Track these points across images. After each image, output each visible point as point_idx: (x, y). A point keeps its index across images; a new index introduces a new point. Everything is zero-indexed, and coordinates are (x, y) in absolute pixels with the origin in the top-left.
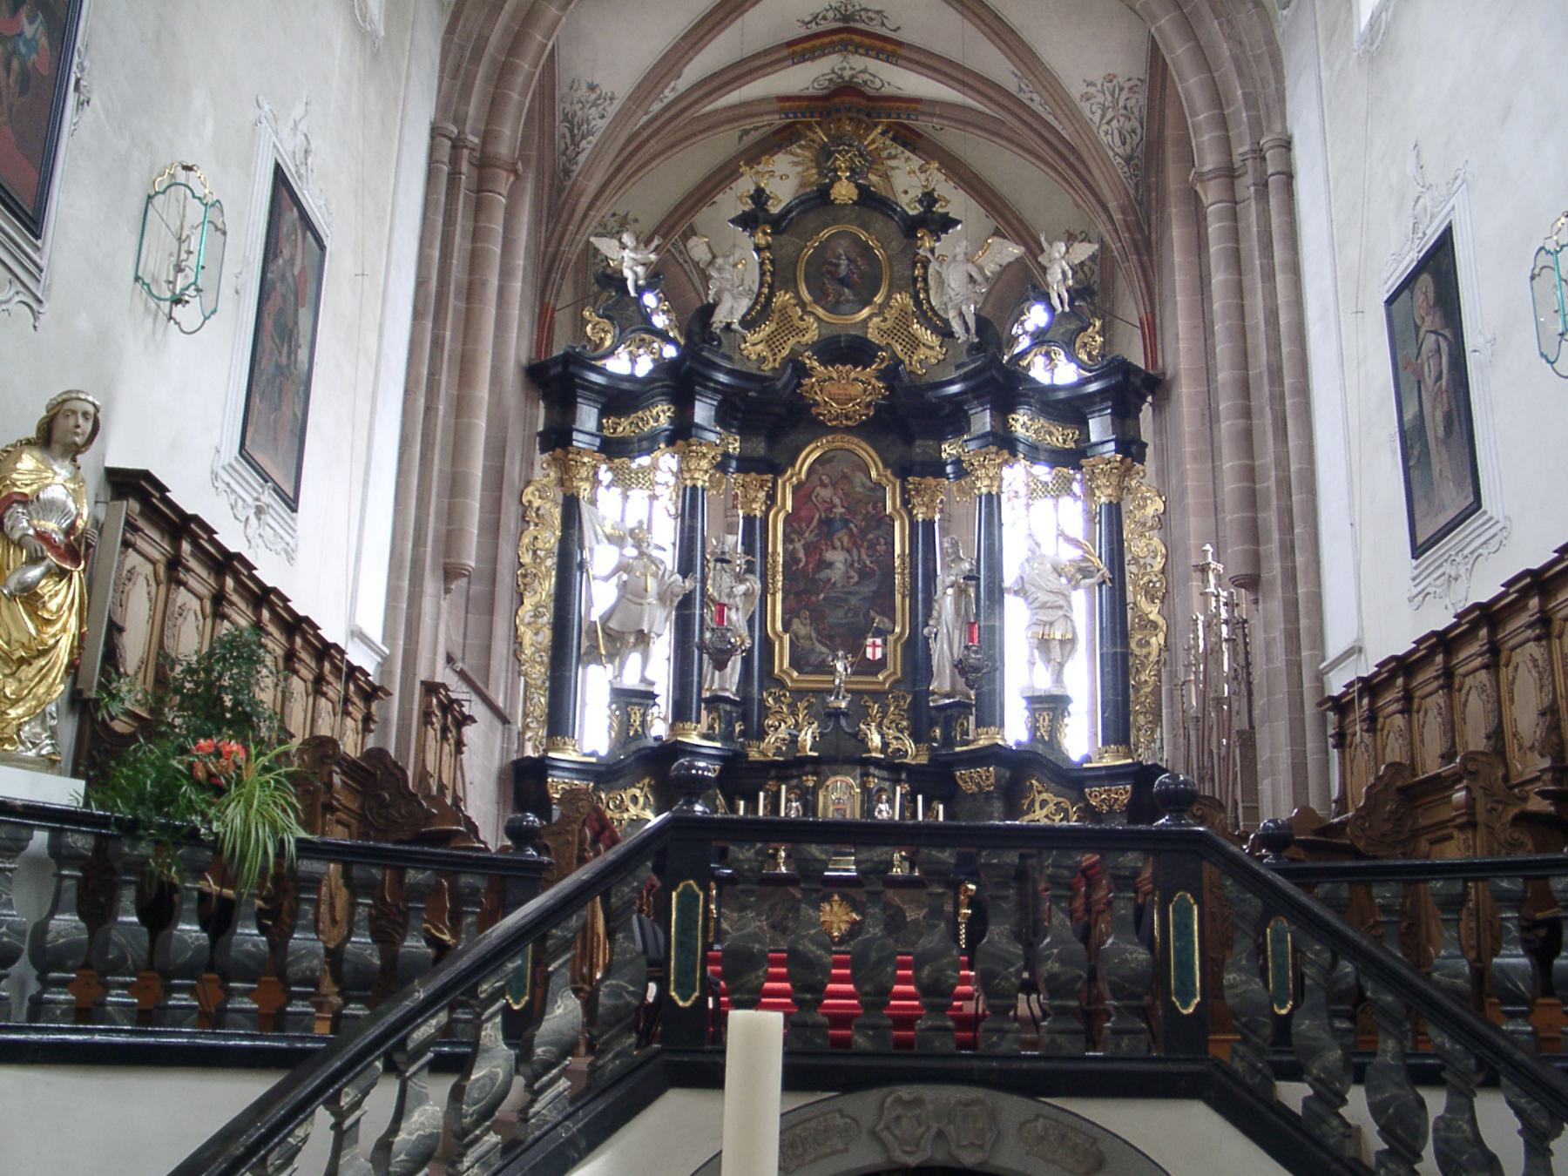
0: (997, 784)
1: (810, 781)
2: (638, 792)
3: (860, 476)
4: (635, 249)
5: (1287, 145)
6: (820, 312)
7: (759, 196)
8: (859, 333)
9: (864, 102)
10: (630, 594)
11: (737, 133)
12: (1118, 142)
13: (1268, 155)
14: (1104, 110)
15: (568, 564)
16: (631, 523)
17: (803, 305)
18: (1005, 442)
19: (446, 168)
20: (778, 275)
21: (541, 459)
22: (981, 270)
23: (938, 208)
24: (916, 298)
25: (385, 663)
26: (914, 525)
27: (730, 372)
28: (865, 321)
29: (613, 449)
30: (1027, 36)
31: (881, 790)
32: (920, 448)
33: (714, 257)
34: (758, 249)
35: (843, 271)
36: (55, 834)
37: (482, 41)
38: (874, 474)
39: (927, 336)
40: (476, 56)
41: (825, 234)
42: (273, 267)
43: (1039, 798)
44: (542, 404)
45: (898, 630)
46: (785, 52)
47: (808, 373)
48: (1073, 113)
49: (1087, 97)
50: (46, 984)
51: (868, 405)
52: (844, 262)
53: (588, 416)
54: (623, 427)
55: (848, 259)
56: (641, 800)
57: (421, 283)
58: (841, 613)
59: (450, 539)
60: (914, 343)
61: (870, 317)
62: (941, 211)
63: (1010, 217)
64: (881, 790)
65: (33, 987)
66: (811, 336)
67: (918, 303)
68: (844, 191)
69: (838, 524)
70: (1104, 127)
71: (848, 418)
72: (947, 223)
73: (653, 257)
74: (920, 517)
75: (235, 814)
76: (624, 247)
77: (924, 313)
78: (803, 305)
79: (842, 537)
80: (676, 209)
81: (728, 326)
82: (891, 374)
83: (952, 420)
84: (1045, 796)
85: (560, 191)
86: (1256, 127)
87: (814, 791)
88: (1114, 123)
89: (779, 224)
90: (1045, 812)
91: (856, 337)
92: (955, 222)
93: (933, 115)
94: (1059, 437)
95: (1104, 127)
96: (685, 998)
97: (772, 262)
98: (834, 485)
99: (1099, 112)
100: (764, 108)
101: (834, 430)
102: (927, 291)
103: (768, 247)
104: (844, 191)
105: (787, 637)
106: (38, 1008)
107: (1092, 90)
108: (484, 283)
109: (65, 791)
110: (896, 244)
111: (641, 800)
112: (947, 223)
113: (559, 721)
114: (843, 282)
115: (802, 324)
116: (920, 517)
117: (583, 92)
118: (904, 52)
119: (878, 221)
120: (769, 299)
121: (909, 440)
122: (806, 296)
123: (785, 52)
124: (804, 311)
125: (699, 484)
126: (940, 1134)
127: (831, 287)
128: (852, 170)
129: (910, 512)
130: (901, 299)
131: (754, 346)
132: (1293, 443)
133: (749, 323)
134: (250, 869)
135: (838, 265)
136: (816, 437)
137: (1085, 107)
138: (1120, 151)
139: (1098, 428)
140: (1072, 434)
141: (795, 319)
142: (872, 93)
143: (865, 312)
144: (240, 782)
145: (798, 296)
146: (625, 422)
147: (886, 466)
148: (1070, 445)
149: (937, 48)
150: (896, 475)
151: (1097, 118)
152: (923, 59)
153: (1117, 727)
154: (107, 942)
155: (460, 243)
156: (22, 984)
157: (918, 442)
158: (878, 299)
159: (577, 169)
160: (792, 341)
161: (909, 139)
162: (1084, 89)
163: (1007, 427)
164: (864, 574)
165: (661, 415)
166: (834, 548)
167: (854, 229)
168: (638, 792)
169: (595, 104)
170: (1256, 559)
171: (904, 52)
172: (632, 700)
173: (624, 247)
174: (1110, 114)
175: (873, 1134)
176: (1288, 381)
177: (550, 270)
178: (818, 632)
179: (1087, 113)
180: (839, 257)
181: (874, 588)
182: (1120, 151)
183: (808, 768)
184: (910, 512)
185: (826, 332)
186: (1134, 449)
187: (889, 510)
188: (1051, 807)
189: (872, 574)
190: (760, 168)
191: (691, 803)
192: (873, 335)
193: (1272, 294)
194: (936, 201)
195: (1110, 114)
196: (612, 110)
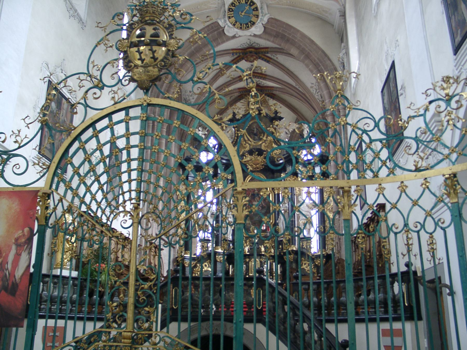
0: (294, 259)
1: (247, 260)
2: (206, 264)
4: (202, 131)
7: (234, 114)
8: (259, 147)
9: (260, 88)
11: (229, 98)
12: (320, 98)
13: (341, 111)
14: (316, 90)
19: (151, 125)
22: (288, 130)
23: (279, 115)
26: (275, 195)
27: (226, 160)
28: (261, 144)
30: (296, 73)
31: (265, 262)
34: (234, 128)
35: (255, 132)
36: (73, 281)
41: (251, 123)
42: (111, 161)
43: (304, 262)
44: (181, 170)
45: (271, 221)
46: (238, 79)
48: (309, 91)
49: (312, 87)
50: (73, 307)
51: (263, 165)
52: (255, 130)
55: (257, 129)
56: (207, 266)
58: (257, 217)
61: (262, 143)
62: (279, 115)
63: (299, 114)
64: (265, 262)
65: (70, 307)
66: (248, 149)
69: (256, 195)
70: (317, 94)
71: (258, 168)
72: (281, 118)
73: (206, 133)
74: (276, 193)
75: (103, 277)
76: (199, 131)
77: (275, 142)
84: (305, 262)
85: (184, 117)
87: (248, 262)
88: (319, 93)
90: (305, 266)
92: (283, 118)
93: (277, 91)
95: (317, 94)
96: (175, 307)
99: (315, 91)
100: (235, 91)
103: (236, 127)
106: (71, 310)
107: (313, 85)
109: (75, 274)
111: (207, 266)
112: (281, 118)
113: (187, 246)
115: (245, 146)
116: (276, 193)
117: (188, 93)
118: (267, 77)
123: (238, 79)
124: (246, 143)
125: (220, 188)
126: (216, 329)
129: (274, 191)
130: (270, 138)
134: (251, 265)
135: (254, 130)
137: (311, 90)
138: (321, 100)
141: (243, 144)
142: (261, 85)
144: (104, 271)
149: (275, 76)
151: (314, 92)
152: (272, 79)
153: (323, 243)
154: (82, 300)
156: (69, 307)
157: (275, 174)
160: (243, 150)
161: (273, 96)
162: (311, 85)
164: (263, 207)
166: (255, 201)
168: (206, 264)
169: (191, 96)
171: (267, 77)
173: (199, 131)
174: (318, 91)
175: (206, 329)
177: (182, 137)
178: (252, 222)
179: (312, 91)
180: (254, 128)
181: (265, 211)
182: (321, 100)
183: (247, 257)
184: (274, 191)
186: (326, 175)
188: (307, 265)
189: (265, 207)
190: (234, 107)
191: (177, 274)
192: (263, 148)
194: (278, 113)
195: (318, 91)
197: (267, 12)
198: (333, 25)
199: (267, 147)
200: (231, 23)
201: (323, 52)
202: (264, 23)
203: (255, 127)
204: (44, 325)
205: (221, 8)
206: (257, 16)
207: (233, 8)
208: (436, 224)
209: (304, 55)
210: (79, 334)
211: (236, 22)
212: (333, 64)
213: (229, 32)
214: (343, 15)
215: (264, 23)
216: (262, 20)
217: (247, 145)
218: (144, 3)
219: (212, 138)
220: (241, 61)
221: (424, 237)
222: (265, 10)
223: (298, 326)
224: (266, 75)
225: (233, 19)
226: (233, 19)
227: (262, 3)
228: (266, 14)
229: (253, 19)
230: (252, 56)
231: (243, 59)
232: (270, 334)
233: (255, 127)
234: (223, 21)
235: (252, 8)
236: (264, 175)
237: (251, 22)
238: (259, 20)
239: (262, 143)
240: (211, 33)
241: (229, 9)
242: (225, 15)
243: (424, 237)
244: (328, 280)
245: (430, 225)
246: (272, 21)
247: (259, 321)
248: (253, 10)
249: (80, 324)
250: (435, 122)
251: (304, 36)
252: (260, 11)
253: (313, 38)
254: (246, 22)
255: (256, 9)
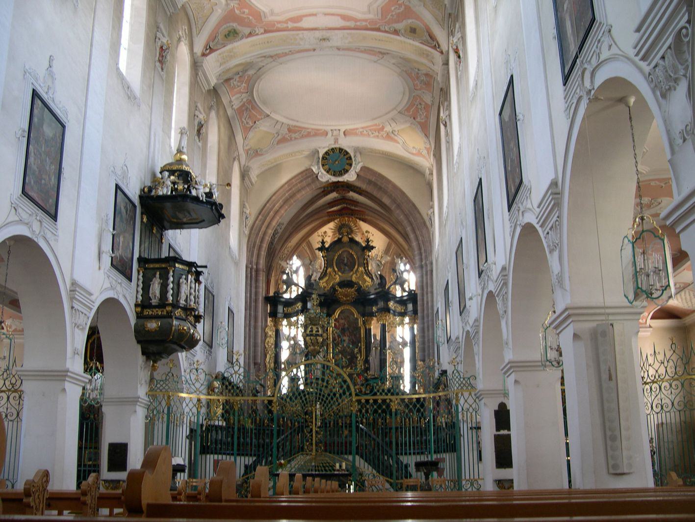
3: (352, 316)
5: (432, 263)
6: (340, 274)
10: (293, 353)
15: (277, 345)
16: (292, 335)
17: (335, 272)
18: (387, 310)
20: (329, 263)
21: (269, 319)
23: (371, 244)
24: (365, 268)
25: (244, 386)
26: (366, 329)
29: (287, 316)
32: (368, 309)
33: (311, 262)
35: (345, 261)
37: (255, 242)
38: (355, 316)
39: (368, 279)
40: (254, 247)
47: (337, 291)
52: (346, 259)
53: (280, 309)
54: (290, 310)
57: (246, 302)
59: (255, 357)
60: (365, 281)
66: (338, 279)
67: (365, 270)
68: (345, 239)
72: (373, 248)
78: (335, 272)
79: (347, 333)
80: (301, 239)
81: (315, 280)
82: (359, 290)
83: (374, 302)
86: (426, 257)
89: (327, 249)
91: (349, 281)
94: (399, 309)
97: (327, 261)
98: (345, 319)
101: (345, 304)
102: (368, 267)
103: (326, 256)
104: (345, 239)
105: (334, 361)
108: (259, 299)
110: (359, 254)
114: (345, 265)
119: (355, 247)
120: (326, 271)
121: (364, 307)
122: (336, 269)
127: (342, 267)
128: (347, 232)
130: (361, 269)
131: (322, 284)
132: (430, 332)
133: (320, 279)
136: (340, 306)
139: (410, 307)
140: (404, 308)
143: (351, 273)
145: (334, 269)
146: (290, 309)
147: (358, 313)
148: (403, 311)
150: (361, 315)
155: (253, 285)
158: (354, 270)
159: (275, 243)
163: (388, 305)
165: (299, 306)
167: (347, 249)
170: (424, 356)
172: (294, 380)
176: (430, 318)
185: (342, 279)
187: (359, 325)
192: (354, 279)
193: (427, 298)
196: (283, 227)
197: (360, 160)
198: (424, 175)
199: (359, 278)
200: (325, 170)
201: (414, 205)
202: (357, 171)
203: (345, 256)
204: (70, 370)
205: (315, 154)
206: (351, 165)
207: (327, 157)
208: (473, 410)
209: (395, 205)
210: (247, 463)
211: (330, 169)
212: (422, 218)
213: (322, 178)
214: (431, 174)
215: (357, 171)
216: (355, 168)
217: (337, 276)
218: (284, 282)
219: (295, 257)
220: (332, 192)
221: (469, 414)
222: (359, 158)
223: (381, 457)
224: (358, 202)
225: (327, 167)
226: (327, 167)
227: (355, 152)
228: (359, 163)
229: (347, 167)
230: (344, 190)
231: (334, 191)
232: (361, 459)
233: (345, 256)
234: (316, 167)
235: (346, 157)
236: (355, 308)
237: (344, 169)
238: (352, 168)
239: (353, 274)
240: (305, 179)
241: (323, 158)
242: (318, 162)
243: (469, 414)
244: (382, 211)
245: (471, 410)
246: (364, 168)
247: (357, 453)
248: (347, 159)
249: (247, 458)
250: (552, 194)
251: (395, 187)
252: (353, 159)
253: (404, 190)
254: (340, 170)
255: (350, 158)
